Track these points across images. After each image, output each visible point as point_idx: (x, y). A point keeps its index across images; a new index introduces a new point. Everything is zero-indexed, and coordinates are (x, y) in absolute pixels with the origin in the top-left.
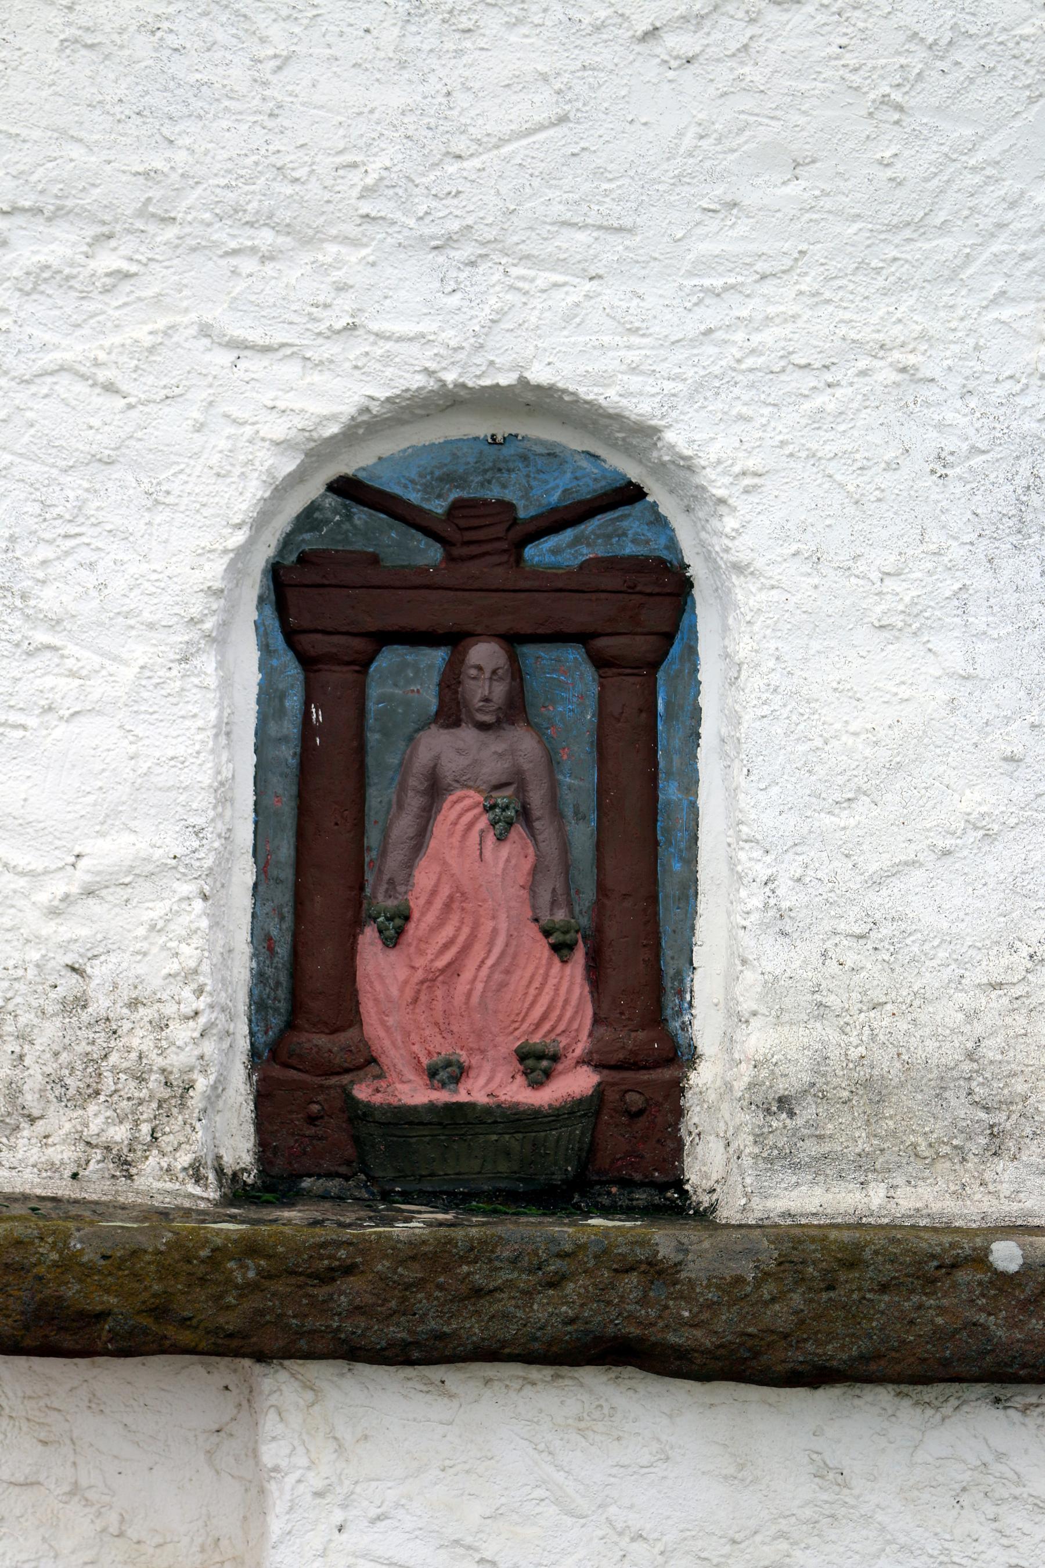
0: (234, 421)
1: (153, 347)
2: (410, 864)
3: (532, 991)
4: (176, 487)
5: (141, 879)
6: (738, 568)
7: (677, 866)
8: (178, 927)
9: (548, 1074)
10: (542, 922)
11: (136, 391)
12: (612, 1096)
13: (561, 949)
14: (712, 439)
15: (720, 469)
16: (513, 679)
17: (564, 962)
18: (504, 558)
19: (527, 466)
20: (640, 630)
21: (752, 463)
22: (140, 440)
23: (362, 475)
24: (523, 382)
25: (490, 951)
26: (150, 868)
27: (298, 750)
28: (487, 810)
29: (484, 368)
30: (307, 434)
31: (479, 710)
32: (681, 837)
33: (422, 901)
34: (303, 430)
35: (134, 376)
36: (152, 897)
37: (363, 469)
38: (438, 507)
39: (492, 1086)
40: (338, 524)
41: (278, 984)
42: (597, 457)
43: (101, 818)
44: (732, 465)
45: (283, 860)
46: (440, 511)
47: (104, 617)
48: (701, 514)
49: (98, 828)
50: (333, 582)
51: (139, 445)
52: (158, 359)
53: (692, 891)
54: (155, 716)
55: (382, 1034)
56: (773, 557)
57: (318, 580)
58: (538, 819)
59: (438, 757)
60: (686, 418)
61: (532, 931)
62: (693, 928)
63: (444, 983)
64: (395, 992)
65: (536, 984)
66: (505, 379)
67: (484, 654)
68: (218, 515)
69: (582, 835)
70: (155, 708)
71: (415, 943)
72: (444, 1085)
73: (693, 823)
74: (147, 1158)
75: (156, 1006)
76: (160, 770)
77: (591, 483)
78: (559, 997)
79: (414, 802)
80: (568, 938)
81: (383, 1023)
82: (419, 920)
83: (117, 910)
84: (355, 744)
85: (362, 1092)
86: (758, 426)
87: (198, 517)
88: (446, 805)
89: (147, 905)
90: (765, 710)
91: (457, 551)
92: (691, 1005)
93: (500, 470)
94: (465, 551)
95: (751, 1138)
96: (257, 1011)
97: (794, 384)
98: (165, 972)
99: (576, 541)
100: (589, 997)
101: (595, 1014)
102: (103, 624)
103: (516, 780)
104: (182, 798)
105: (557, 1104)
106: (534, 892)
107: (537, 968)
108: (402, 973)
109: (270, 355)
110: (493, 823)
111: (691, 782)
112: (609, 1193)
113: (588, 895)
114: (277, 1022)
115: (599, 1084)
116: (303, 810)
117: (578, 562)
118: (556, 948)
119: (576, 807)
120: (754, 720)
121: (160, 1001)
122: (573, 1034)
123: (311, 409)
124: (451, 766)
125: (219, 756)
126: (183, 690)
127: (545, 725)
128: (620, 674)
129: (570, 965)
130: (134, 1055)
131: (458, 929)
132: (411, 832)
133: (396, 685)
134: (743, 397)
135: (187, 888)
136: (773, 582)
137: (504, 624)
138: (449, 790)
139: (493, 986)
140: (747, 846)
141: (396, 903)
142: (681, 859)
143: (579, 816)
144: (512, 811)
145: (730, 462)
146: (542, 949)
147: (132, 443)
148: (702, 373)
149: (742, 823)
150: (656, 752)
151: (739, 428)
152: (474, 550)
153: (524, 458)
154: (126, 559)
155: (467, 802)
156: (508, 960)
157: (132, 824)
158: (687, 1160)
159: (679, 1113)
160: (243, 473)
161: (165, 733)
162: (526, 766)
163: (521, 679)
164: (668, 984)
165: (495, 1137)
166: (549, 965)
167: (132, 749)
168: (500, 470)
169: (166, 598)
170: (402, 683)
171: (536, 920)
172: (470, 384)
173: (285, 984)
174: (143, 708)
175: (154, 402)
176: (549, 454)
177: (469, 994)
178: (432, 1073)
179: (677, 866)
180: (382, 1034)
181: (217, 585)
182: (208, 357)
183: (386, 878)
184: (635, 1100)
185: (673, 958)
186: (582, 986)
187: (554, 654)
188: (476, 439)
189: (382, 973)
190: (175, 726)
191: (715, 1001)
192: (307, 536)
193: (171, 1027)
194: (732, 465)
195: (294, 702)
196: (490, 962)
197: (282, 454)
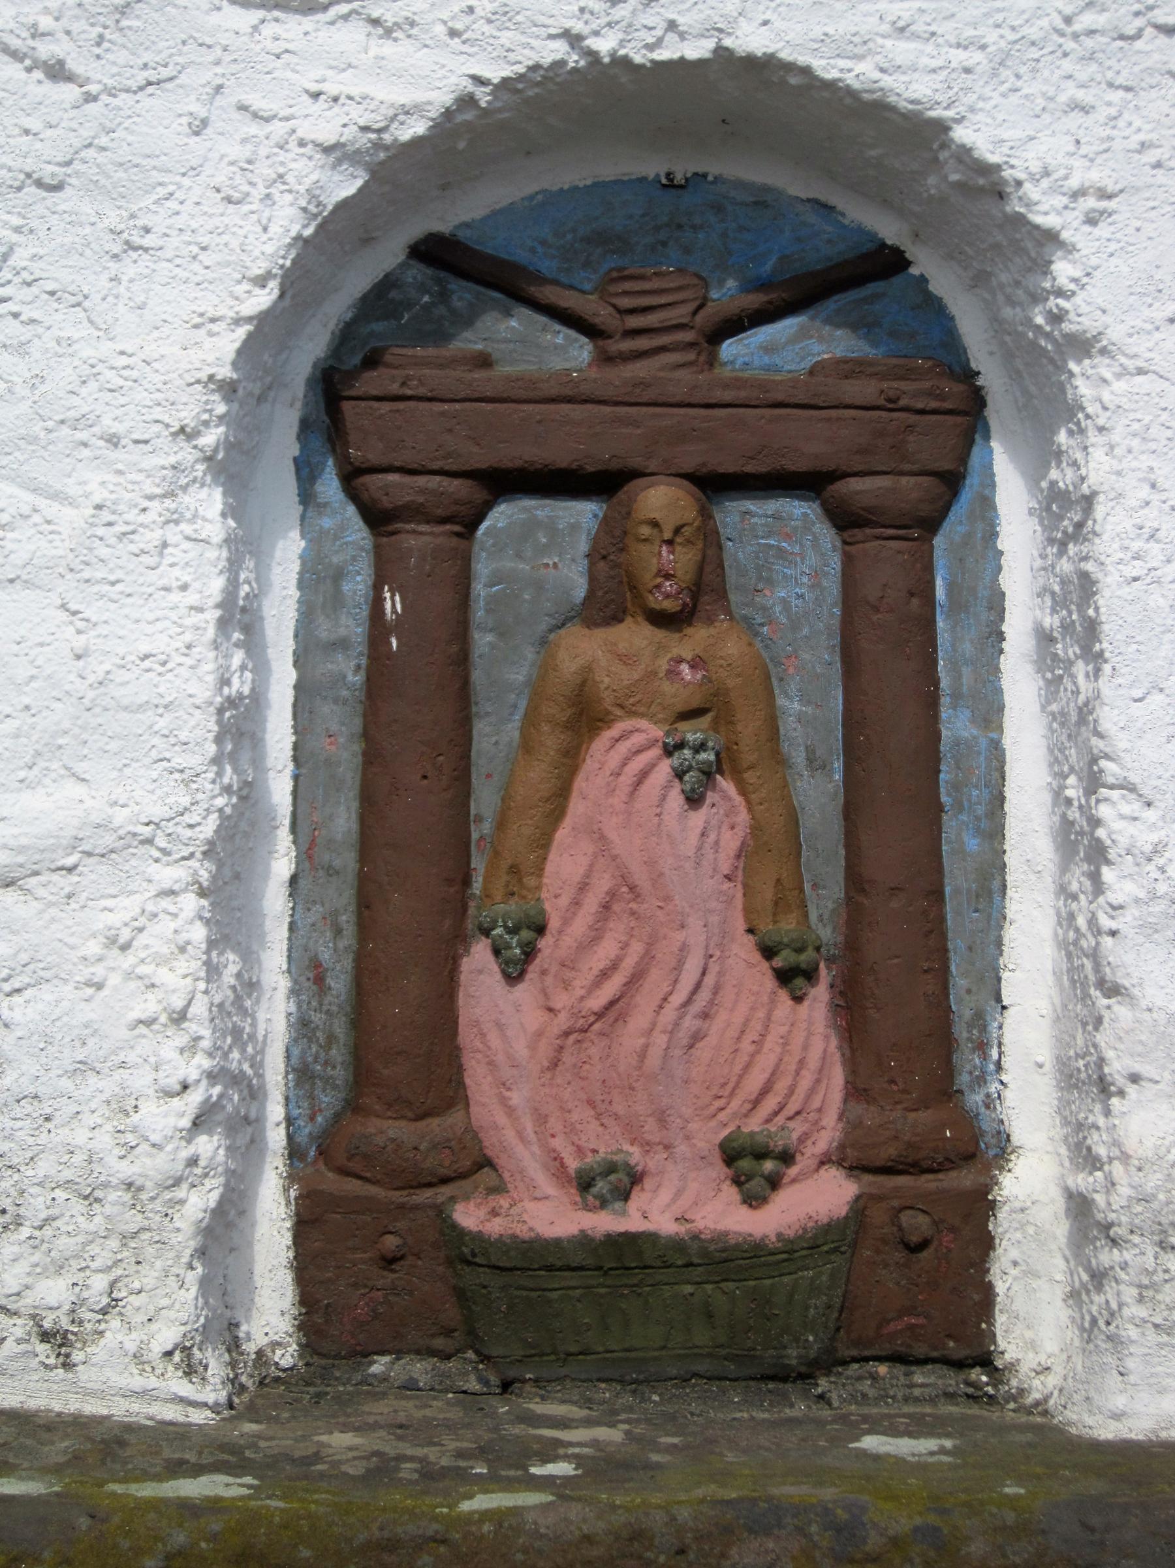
0: (255, 115)
3: (746, 1046)
4: (158, 221)
5: (92, 860)
7: (972, 844)
9: (774, 1183)
11: (97, 73)
12: (878, 1215)
14: (1032, 139)
15: (1045, 183)
17: (798, 999)
18: (691, 356)
20: (907, 467)
21: (1095, 176)
22: (104, 149)
23: (462, 235)
24: (722, 53)
26: (109, 840)
27: (364, 661)
28: (669, 751)
29: (659, 32)
30: (373, 136)
32: (977, 795)
33: (564, 901)
35: (97, 51)
36: (113, 891)
37: (466, 225)
39: (684, 1202)
40: (426, 308)
41: (331, 1038)
42: (832, 208)
43: (28, 759)
44: (1066, 178)
45: (339, 837)
47: (37, 429)
48: (1004, 277)
49: (22, 774)
50: (422, 391)
51: (101, 158)
52: (135, 23)
53: (996, 884)
54: (119, 587)
55: (501, 1119)
56: (1138, 323)
57: (395, 388)
58: (750, 768)
60: (988, 106)
61: (744, 949)
62: (999, 943)
63: (602, 1034)
64: (521, 1049)
66: (697, 50)
67: (660, 499)
68: (228, 264)
69: (818, 795)
70: (119, 574)
72: (603, 1204)
73: (996, 775)
74: (101, 1333)
75: (118, 1075)
76: (127, 676)
80: (804, 959)
81: (504, 1101)
83: (53, 911)
84: (455, 648)
85: (469, 1216)
86: (1102, 120)
87: (196, 266)
90: (1137, 568)
92: (999, 1067)
93: (680, 227)
94: (627, 345)
95: (1134, 1292)
96: (298, 1083)
97: (1156, 56)
98: (136, 1014)
100: (837, 1057)
102: (35, 440)
104: (162, 724)
105: (791, 1233)
108: (534, 1018)
110: (679, 774)
112: (874, 1377)
114: (329, 1100)
115: (858, 1198)
116: (372, 757)
117: (807, 364)
118: (784, 977)
120: (1119, 585)
121: (123, 1065)
122: (813, 1116)
123: (380, 96)
125: (228, 656)
126: (165, 545)
128: (877, 538)
129: (806, 1003)
130: (79, 1158)
131: (625, 946)
133: (519, 556)
134: (1077, 75)
135: (171, 875)
136: (1140, 363)
137: (693, 457)
139: (683, 1036)
142: (978, 831)
144: (719, 743)
145: (1062, 172)
146: (761, 977)
147: (91, 153)
148: (1012, 37)
150: (935, 662)
151: (1076, 118)
152: (643, 343)
154: (76, 336)
155: (637, 740)
156: (704, 996)
158: (1001, 1319)
159: (987, 1243)
160: (268, 196)
162: (731, 683)
164: (960, 1031)
166: (773, 1002)
167: (80, 642)
168: (680, 227)
169: (140, 395)
170: (529, 553)
171: (750, 931)
172: (638, 59)
173: (342, 1038)
174: (99, 575)
176: (756, 203)
178: (585, 1183)
179: (972, 844)
180: (501, 1119)
181: (225, 372)
182: (215, 18)
183: (504, 865)
184: (917, 1223)
185: (969, 991)
186: (827, 1037)
188: (643, 180)
190: (151, 604)
193: (143, 1110)
194: (1066, 178)
195: (358, 584)
196: (678, 999)
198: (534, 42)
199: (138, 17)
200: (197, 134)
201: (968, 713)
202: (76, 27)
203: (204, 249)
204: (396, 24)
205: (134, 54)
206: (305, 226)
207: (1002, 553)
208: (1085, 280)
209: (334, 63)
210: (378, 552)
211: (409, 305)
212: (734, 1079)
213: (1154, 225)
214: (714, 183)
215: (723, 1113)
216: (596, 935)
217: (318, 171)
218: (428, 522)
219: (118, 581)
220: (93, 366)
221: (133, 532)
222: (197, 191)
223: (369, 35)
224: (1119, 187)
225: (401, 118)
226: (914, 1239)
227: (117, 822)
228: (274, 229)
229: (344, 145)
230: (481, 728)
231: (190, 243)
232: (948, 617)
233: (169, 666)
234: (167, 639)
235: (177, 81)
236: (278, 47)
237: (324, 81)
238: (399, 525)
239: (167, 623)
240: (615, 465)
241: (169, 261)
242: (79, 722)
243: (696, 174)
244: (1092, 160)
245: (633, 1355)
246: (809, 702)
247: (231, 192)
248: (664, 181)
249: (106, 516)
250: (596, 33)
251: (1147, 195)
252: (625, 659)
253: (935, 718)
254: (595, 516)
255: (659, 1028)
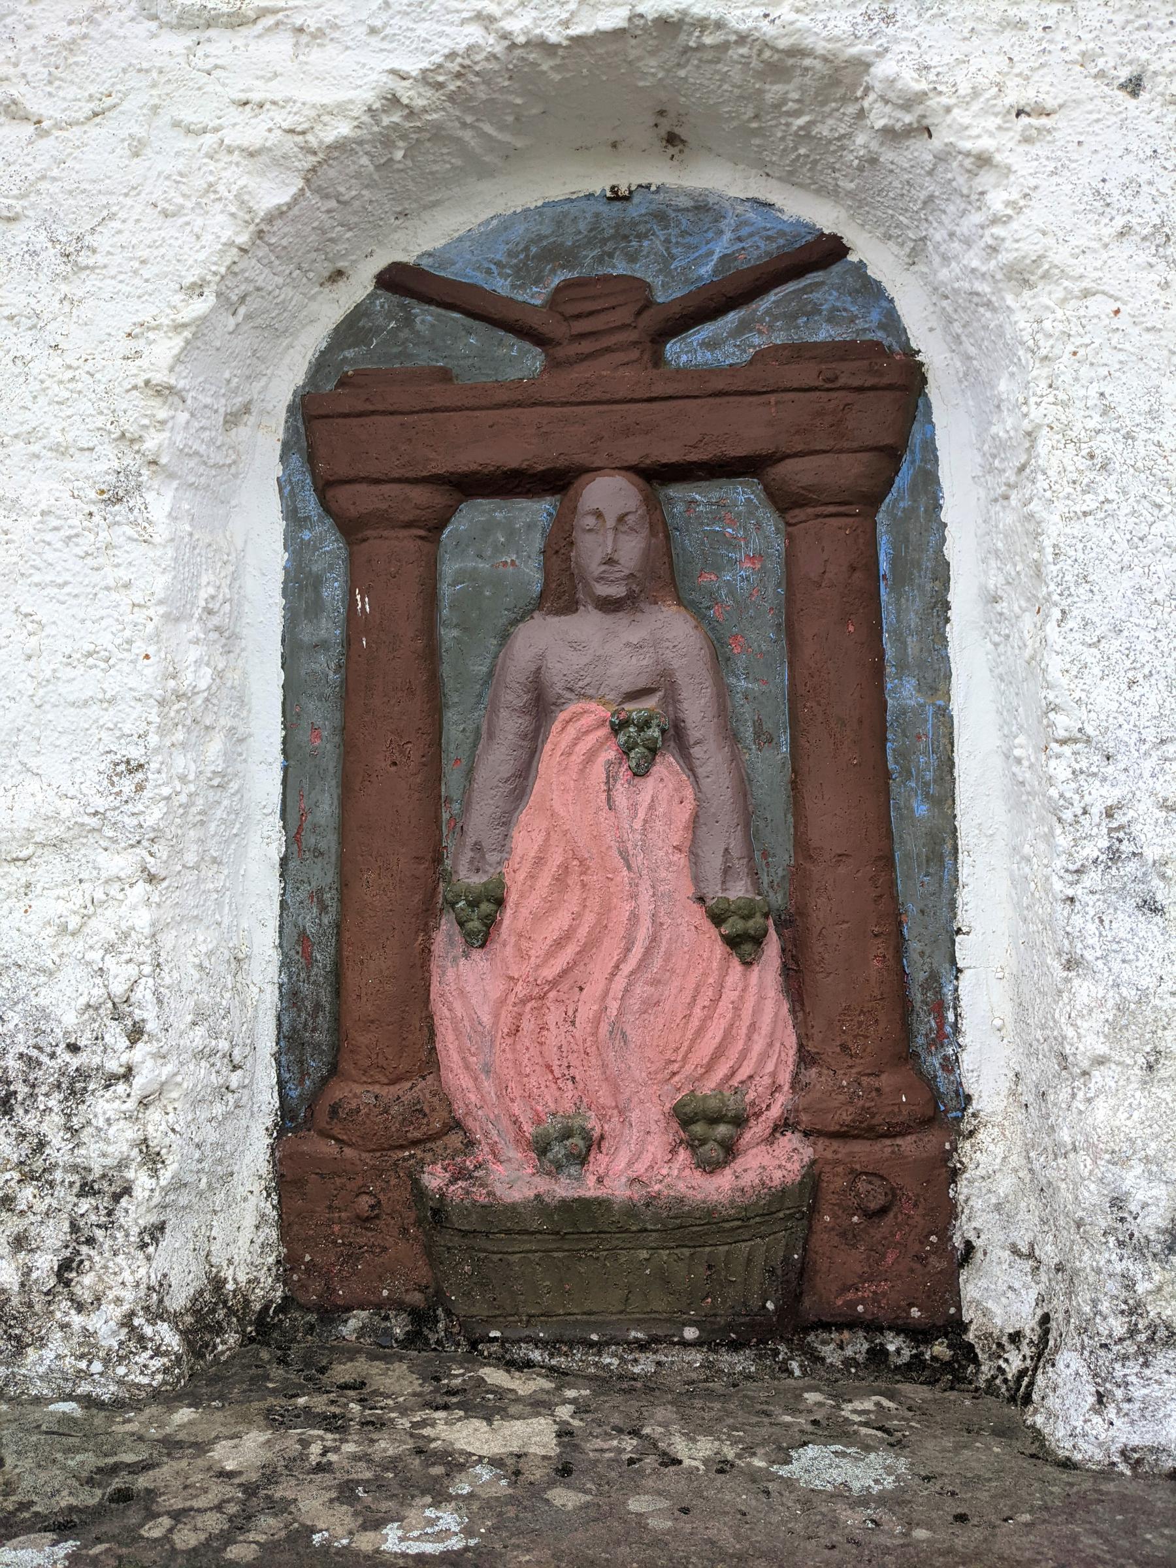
1: (74, 41)
2: (506, 821)
6: (1021, 276)
7: (921, 809)
8: (103, 928)
10: (710, 903)
13: (743, 945)
15: (976, 106)
16: (653, 532)
17: (747, 964)
18: (634, 354)
19: (666, 228)
23: (425, 263)
25: (628, 950)
26: (57, 831)
30: (299, 139)
31: (600, 579)
32: (925, 762)
33: (521, 876)
34: (292, 131)
35: (48, 89)
37: (429, 254)
38: (536, 296)
41: (318, 1007)
45: (323, 822)
46: (538, 302)
51: (54, 188)
52: (81, 58)
53: (948, 847)
54: (67, 589)
55: (466, 1082)
56: (1083, 242)
58: (696, 743)
59: (542, 657)
61: (697, 915)
65: (703, 1001)
67: (608, 493)
70: (67, 577)
71: (513, 939)
77: (762, 244)
78: (747, 1027)
79: (510, 725)
81: (467, 1067)
82: (517, 905)
84: (419, 644)
87: (137, 281)
88: (556, 726)
89: (57, 892)
91: (560, 353)
99: (744, 327)
101: (801, 1047)
103: (662, 684)
106: (696, 855)
107: (705, 974)
109: (244, 31)
110: (626, 750)
111: (936, 675)
113: (783, 857)
115: (813, 1162)
116: (348, 747)
118: (733, 942)
119: (758, 725)
124: (561, 668)
127: (706, 603)
128: (818, 516)
129: (756, 969)
132: (506, 770)
135: (122, 863)
136: (1085, 284)
138: (559, 704)
139: (634, 1003)
140: (1067, 750)
141: (485, 879)
142: (927, 796)
143: (764, 738)
147: (43, 185)
149: (1056, 709)
151: (1007, 39)
152: (586, 347)
153: (661, 217)
155: (586, 721)
157: (33, 763)
161: (81, 615)
162: (676, 663)
163: (667, 537)
165: (644, 1254)
166: (724, 972)
169: (85, 406)
171: (701, 899)
172: (553, 38)
174: (48, 578)
175: (78, 123)
176: (696, 208)
177: (597, 1021)
178: (541, 1147)
179: (921, 809)
187: (715, 496)
189: (468, 988)
191: (998, 1023)
192: (349, 354)
195: (333, 590)
196: (627, 968)
197: (262, 174)
198: (447, 29)
199: (84, 53)
200: (136, 155)
201: (914, 681)
202: (31, 70)
203: (143, 262)
204: (319, 29)
205: (81, 88)
206: (237, 234)
207: (945, 525)
208: (1022, 203)
209: (260, 73)
210: (351, 559)
211: (377, 331)
212: (686, 1044)
213: (1099, 138)
214: (658, 191)
215: (676, 1078)
216: (550, 908)
217: (246, 177)
218: (393, 528)
219: (66, 583)
220: (42, 382)
221: (77, 535)
222: (139, 208)
223: (297, 44)
224: (1056, 103)
225: (326, 118)
226: (873, 1206)
227: (64, 815)
228: (207, 238)
229: (270, 150)
230: (451, 715)
231: (131, 259)
232: (892, 590)
233: (111, 662)
234: (111, 637)
235: (121, 108)
236: (208, 64)
237: (251, 90)
238: (368, 533)
239: (110, 621)
240: (561, 463)
241: (113, 278)
242: (31, 719)
243: (640, 186)
244: (1027, 78)
245: (593, 1318)
246: (756, 680)
247: (166, 205)
248: (609, 194)
249: (53, 522)
250: (510, 13)
251: (1090, 107)
252: (574, 646)
253: (881, 688)
254: (550, 514)
255: (611, 994)
